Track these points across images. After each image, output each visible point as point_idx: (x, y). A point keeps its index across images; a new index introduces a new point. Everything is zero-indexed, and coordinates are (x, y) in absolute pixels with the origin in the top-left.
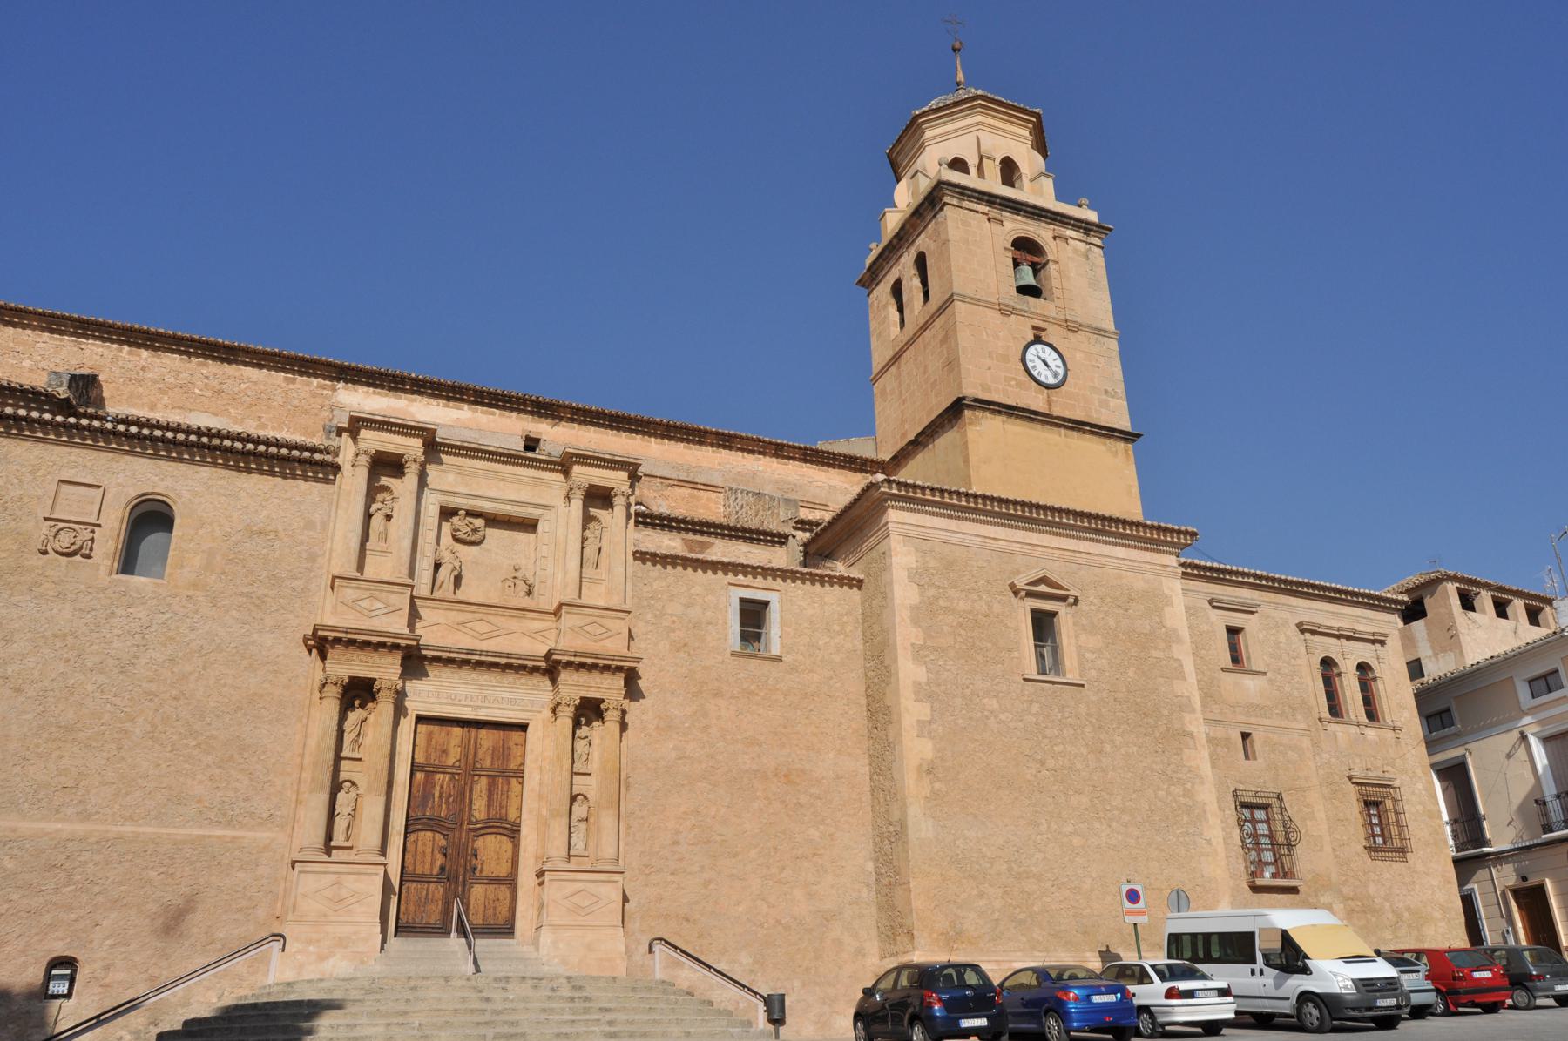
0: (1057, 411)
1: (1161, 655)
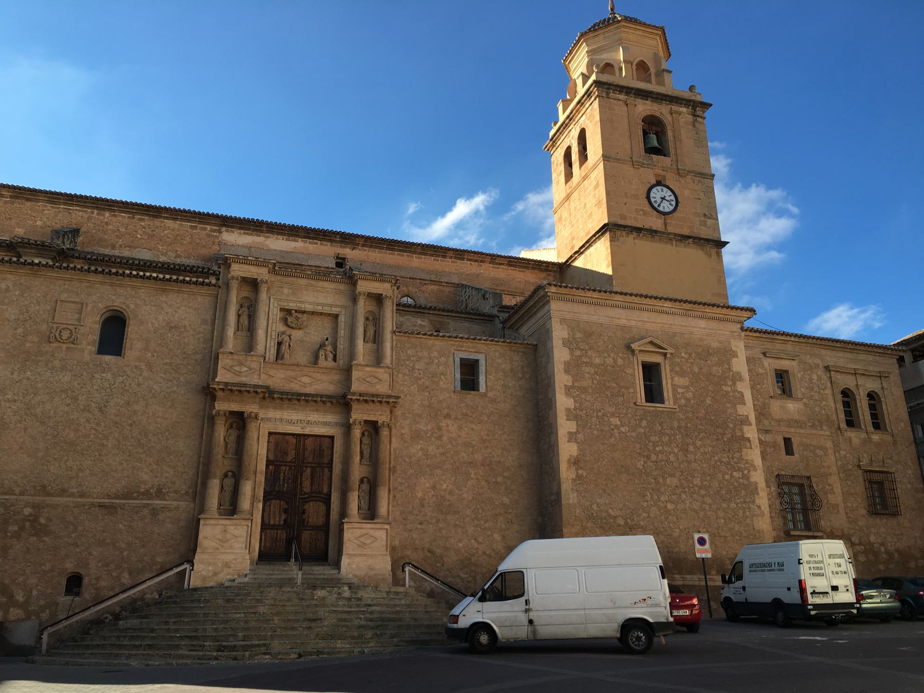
0: (670, 229)
1: (729, 389)
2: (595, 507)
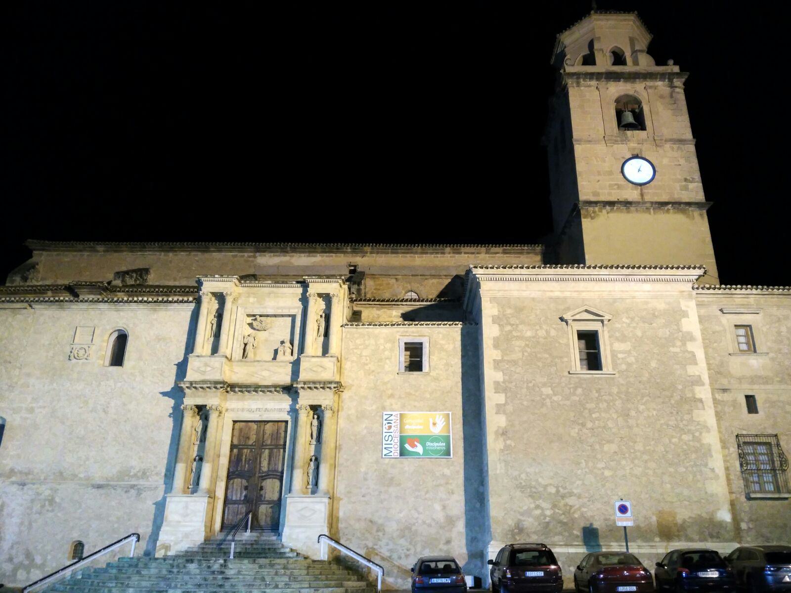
0: (647, 198)
1: (678, 350)
2: (523, 476)
